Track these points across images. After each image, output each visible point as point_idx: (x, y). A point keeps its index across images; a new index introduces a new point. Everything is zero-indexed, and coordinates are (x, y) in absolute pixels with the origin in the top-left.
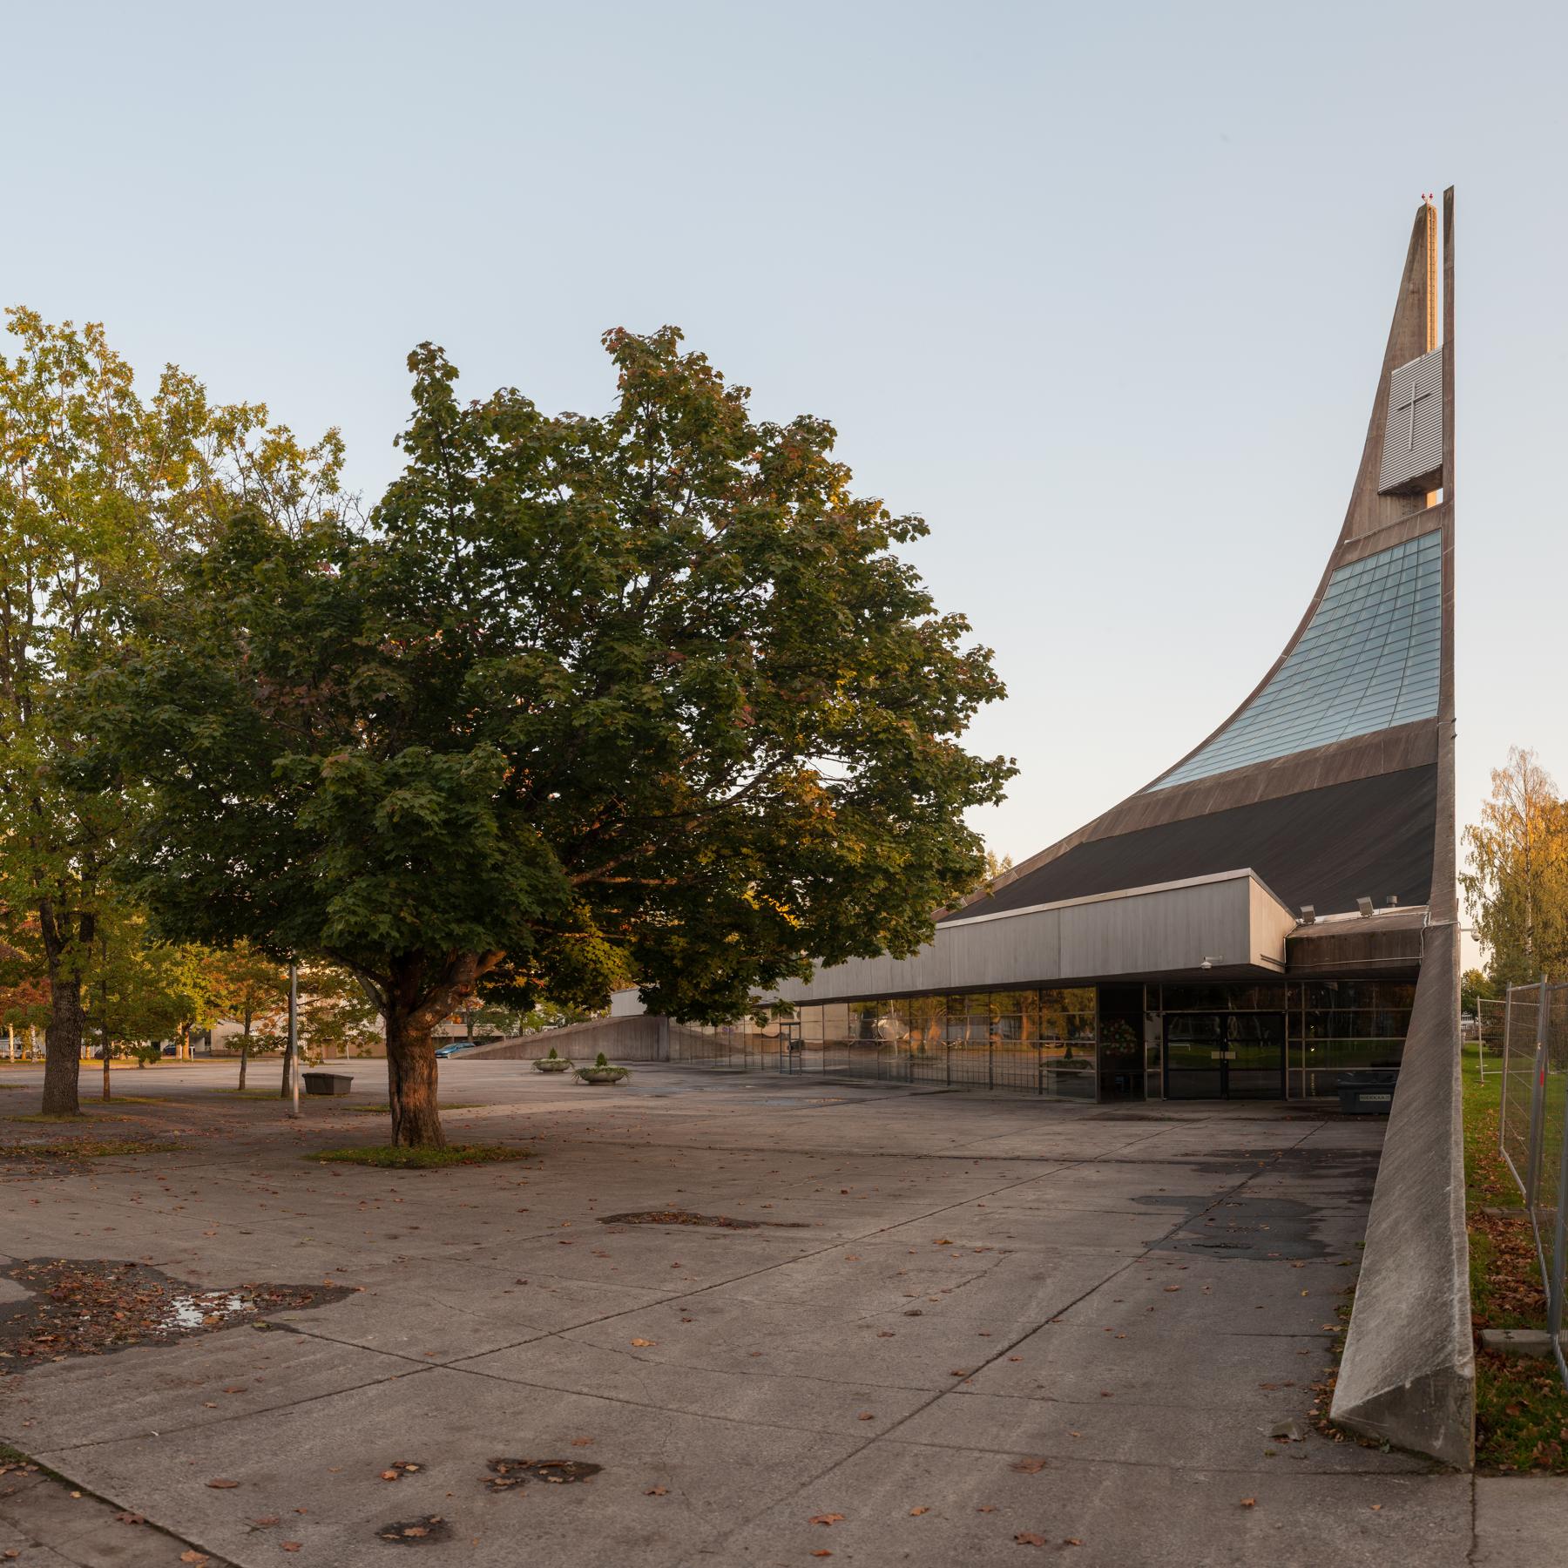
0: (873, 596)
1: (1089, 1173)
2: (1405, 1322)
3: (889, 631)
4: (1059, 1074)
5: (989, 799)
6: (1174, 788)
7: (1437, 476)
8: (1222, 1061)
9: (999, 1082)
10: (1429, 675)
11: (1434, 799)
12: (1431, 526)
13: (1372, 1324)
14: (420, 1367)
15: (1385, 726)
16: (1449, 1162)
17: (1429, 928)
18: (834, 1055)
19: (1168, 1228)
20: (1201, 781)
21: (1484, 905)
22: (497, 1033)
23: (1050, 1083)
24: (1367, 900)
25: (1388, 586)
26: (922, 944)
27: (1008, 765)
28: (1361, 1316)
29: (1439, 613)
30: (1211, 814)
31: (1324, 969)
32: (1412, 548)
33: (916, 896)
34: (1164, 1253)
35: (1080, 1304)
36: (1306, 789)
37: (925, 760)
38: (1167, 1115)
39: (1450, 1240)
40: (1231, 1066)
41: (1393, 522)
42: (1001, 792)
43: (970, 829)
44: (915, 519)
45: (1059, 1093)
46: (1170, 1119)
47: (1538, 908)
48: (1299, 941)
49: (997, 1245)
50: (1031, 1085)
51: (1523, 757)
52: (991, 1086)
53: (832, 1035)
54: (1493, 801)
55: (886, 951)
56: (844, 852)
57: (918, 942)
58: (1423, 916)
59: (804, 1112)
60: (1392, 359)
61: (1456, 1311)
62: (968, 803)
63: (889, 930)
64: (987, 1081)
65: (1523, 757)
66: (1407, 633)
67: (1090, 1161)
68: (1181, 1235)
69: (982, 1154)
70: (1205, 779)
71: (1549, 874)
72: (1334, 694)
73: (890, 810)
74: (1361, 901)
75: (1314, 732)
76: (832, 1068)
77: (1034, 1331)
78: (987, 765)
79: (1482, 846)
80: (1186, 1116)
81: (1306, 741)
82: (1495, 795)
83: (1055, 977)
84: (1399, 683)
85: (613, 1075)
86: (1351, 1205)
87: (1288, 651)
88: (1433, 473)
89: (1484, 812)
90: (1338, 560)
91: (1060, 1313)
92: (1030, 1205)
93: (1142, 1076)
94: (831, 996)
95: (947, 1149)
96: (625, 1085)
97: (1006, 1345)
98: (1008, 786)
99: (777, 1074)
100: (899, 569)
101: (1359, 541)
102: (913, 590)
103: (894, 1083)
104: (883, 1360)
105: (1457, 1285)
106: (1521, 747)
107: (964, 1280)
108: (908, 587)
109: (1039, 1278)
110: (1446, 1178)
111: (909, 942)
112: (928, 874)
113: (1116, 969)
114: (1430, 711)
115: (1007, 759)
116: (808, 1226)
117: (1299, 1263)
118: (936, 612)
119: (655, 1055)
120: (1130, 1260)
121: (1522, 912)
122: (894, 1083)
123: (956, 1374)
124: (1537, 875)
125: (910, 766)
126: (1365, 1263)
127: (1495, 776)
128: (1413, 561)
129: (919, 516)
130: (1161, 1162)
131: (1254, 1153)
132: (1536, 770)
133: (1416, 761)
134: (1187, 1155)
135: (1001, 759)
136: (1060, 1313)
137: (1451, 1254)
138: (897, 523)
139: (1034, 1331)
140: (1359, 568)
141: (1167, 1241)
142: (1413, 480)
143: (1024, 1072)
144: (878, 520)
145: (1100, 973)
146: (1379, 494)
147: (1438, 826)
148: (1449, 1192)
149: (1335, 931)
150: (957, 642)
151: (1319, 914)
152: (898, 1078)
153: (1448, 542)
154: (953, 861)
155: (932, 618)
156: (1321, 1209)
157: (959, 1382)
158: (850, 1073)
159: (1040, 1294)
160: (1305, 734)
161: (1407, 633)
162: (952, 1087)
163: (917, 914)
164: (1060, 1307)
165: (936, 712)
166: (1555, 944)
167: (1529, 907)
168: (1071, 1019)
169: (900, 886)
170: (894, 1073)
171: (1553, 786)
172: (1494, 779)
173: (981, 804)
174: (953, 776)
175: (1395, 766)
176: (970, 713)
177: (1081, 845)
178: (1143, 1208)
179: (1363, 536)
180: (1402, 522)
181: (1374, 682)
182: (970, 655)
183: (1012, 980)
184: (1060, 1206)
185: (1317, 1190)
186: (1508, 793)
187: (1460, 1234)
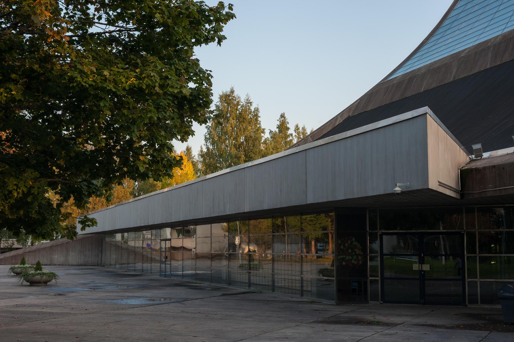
5: (213, 40)
6: (403, 75)
14: (377, 332)
20: (419, 69)
22: (16, 245)
30: (425, 92)
31: (489, 194)
36: (482, 69)
42: (222, 33)
46: (378, 323)
48: (471, 170)
52: (273, 288)
56: (76, 74)
62: (198, 43)
70: (421, 68)
75: (488, 29)
78: (211, 9)
81: (482, 36)
83: (304, 203)
85: (45, 278)
93: (366, 283)
96: (54, 286)
98: (227, 29)
115: (226, 4)
119: (100, 262)
149: (495, 162)
151: (485, 151)
154: (172, 87)
160: (481, 32)
162: (252, 289)
173: (207, 43)
177: (349, 117)
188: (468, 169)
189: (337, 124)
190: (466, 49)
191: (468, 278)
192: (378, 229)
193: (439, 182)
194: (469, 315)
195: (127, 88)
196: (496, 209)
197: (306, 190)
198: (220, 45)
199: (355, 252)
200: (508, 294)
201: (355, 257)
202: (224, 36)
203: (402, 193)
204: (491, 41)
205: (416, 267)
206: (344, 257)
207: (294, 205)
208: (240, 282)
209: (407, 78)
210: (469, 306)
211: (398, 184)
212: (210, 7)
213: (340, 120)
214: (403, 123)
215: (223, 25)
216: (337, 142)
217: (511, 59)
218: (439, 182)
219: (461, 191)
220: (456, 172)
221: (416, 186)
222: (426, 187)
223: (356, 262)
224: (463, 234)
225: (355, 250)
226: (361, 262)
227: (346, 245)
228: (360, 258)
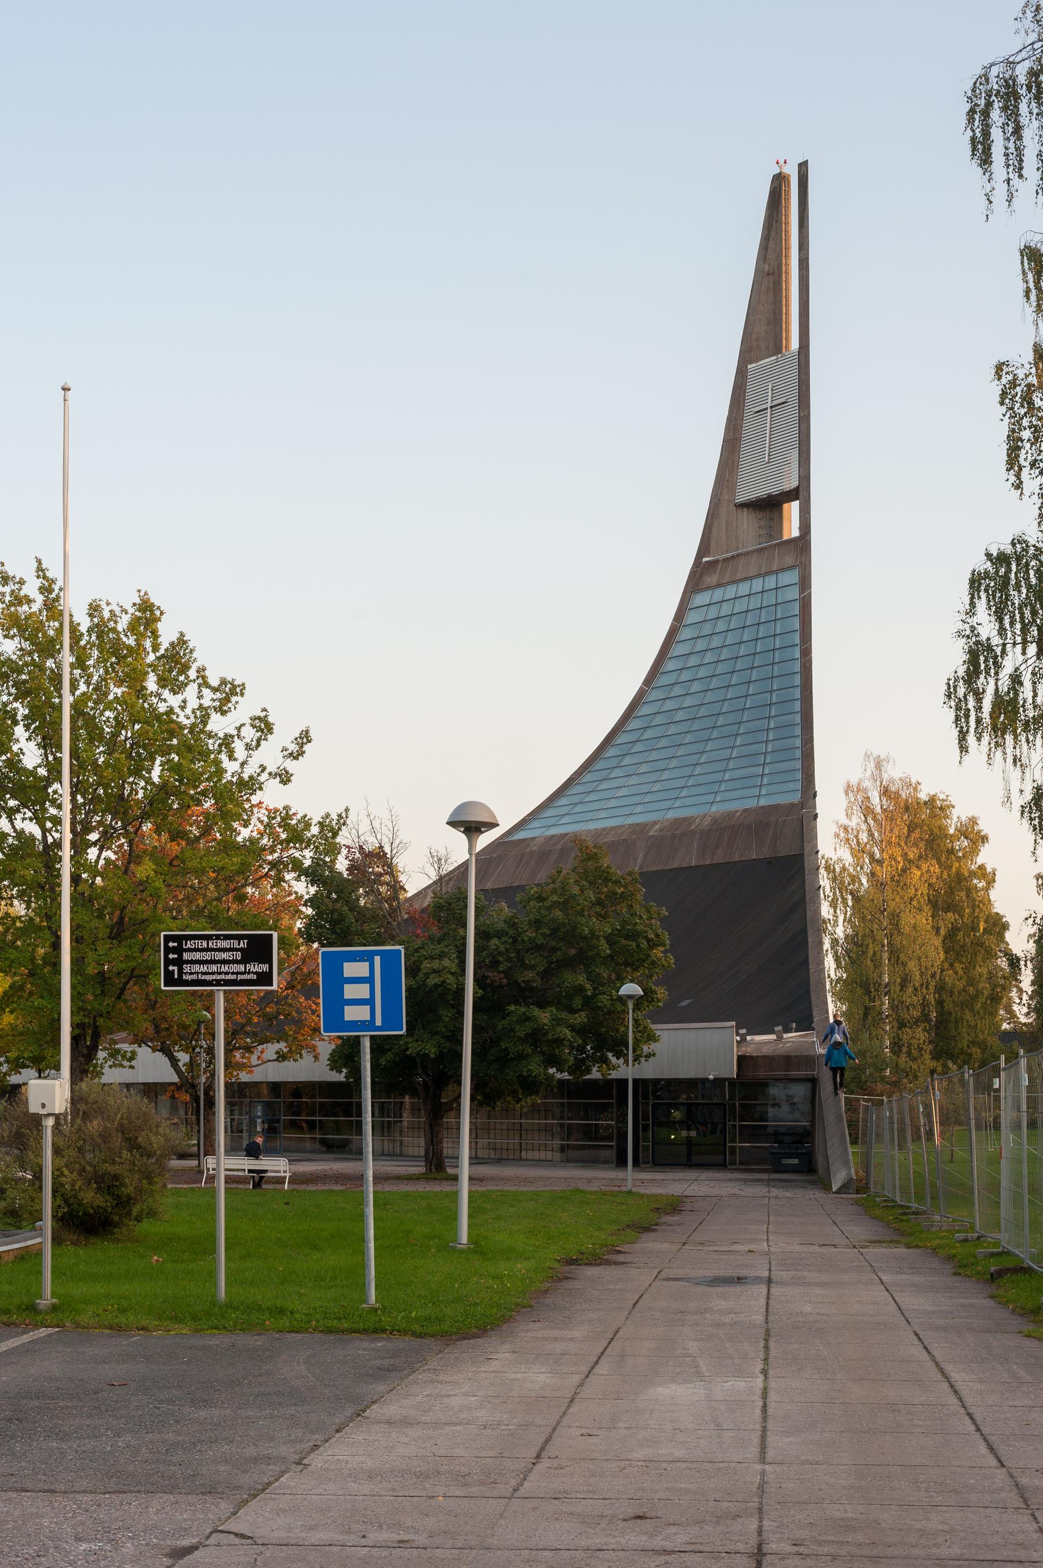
36: (685, 865)
51: (879, 765)
54: (845, 821)
60: (749, 352)
65: (879, 765)
87: (649, 681)
89: (837, 836)
90: (696, 581)
101: (716, 562)
114: (796, 797)
121: (877, 964)
153: (805, 583)
172: (847, 794)
175: (765, 853)
210: (729, 1167)
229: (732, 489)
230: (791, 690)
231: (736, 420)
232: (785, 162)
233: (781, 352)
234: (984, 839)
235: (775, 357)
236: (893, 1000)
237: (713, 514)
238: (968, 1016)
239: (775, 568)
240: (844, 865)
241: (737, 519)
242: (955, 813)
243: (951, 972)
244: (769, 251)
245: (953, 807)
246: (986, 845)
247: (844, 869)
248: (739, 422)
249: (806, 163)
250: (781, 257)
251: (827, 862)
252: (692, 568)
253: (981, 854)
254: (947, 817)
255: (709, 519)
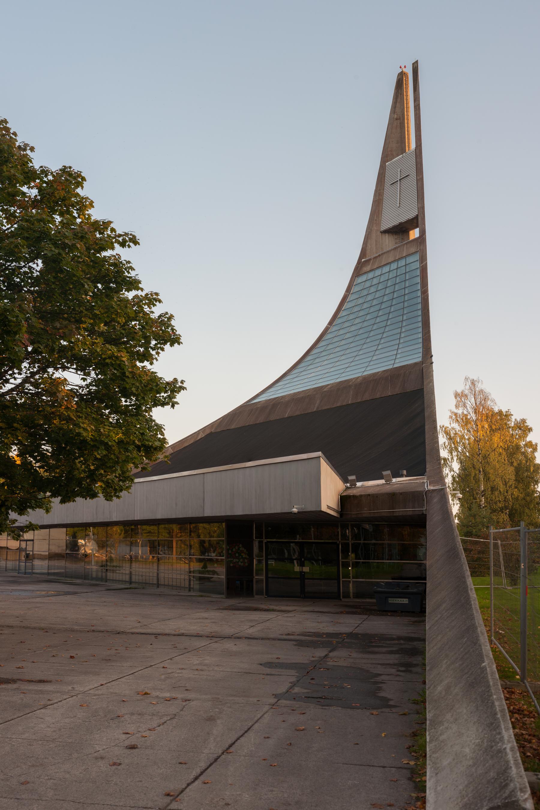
0: (104, 276)
1: (229, 645)
2: (471, 763)
3: (113, 298)
4: (201, 579)
5: (167, 404)
6: (267, 401)
7: (415, 221)
8: (301, 572)
9: (162, 583)
10: (415, 336)
11: (423, 411)
12: (413, 250)
13: (445, 763)
15: (391, 367)
16: (480, 646)
17: (429, 491)
18: (56, 563)
19: (287, 685)
21: (453, 476)
23: (196, 585)
24: (388, 472)
25: (389, 285)
26: (123, 492)
27: (180, 384)
28: (434, 755)
29: (419, 300)
30: (289, 418)
32: (402, 263)
33: (124, 461)
34: (288, 702)
35: (242, 739)
36: (344, 404)
37: (133, 377)
38: (272, 607)
39: (493, 703)
40: (306, 577)
41: (390, 249)
42: (175, 400)
43: (157, 422)
44: (131, 235)
45: (201, 590)
46: (274, 610)
47: (487, 479)
49: (180, 696)
50: (183, 585)
53: (55, 549)
55: (101, 495)
56: (81, 430)
57: (121, 490)
58: (424, 483)
59: (38, 600)
60: (387, 156)
61: (510, 756)
62: (155, 405)
63: (103, 481)
64: (155, 582)
65: (473, 383)
66: (401, 312)
67: (229, 637)
68: (296, 690)
69: (159, 631)
71: (492, 456)
72: (359, 348)
73: (106, 407)
74: (384, 473)
76: (53, 571)
77: (216, 760)
78: (168, 383)
79: (450, 439)
80: (283, 608)
81: (343, 375)
82: (457, 407)
83: (201, 515)
84: (397, 342)
86: (399, 673)
87: (331, 323)
88: (413, 219)
89: (451, 417)
90: (358, 271)
91: (230, 746)
92: (196, 667)
93: (252, 581)
94: (56, 523)
95: (136, 627)
97: (198, 771)
98: (179, 397)
99: (16, 574)
100: (121, 262)
102: (129, 275)
103: (94, 582)
104: (116, 784)
105: (506, 737)
106: (471, 378)
107: (162, 721)
108: (126, 274)
109: (211, 719)
110: (481, 657)
111: (115, 490)
112: (131, 448)
113: (239, 511)
114: (417, 358)
115: (179, 380)
116: (50, 682)
117: (375, 712)
118: (142, 290)
120: (266, 708)
121: (477, 481)
122: (94, 582)
123: (168, 795)
124: (485, 457)
125: (124, 380)
126: (429, 716)
127: (456, 395)
128: (403, 270)
129: (133, 233)
130: (274, 639)
131: (329, 635)
132: (481, 391)
133: (411, 387)
134: (289, 634)
135: (176, 380)
136: (230, 746)
137: (496, 714)
138: (120, 236)
139: (216, 760)
140: (371, 275)
141: (286, 695)
142: (401, 224)
143: (178, 577)
144: (109, 232)
145: (229, 514)
146: (381, 232)
147: (427, 427)
148: (485, 667)
149: (370, 491)
150: (153, 309)
152: (97, 579)
153: (423, 259)
154: (148, 440)
155: (139, 293)
156: (381, 675)
157: (171, 801)
158: (66, 575)
159: (215, 732)
161: (401, 312)
162: (133, 585)
163: (123, 472)
164: (230, 742)
165: (138, 349)
166: (500, 501)
167: (481, 477)
168: (202, 543)
169: (114, 455)
170: (94, 575)
171: (493, 401)
172: (456, 397)
174: (148, 388)
175: (398, 390)
176: (159, 351)
177: (211, 434)
178: (268, 671)
179: (372, 257)
180: (395, 249)
181: (382, 341)
182: (160, 316)
183: (174, 517)
184: (216, 668)
185: (374, 662)
186: (465, 406)
187: (499, 699)
188: (346, 496)
189: (199, 438)
190: (328, 385)
191: (342, 578)
192: (264, 538)
193: (327, 506)
194: (346, 606)
195: (117, 441)
196: (365, 525)
197: (204, 506)
198: (173, 408)
199: (242, 556)
200: (380, 589)
201: (241, 560)
202: (177, 402)
203: (298, 512)
204: (352, 381)
205: (297, 569)
206: (232, 559)
207: (190, 516)
208: (113, 580)
209: (271, 404)
210: (343, 600)
211: (295, 506)
212: (167, 381)
213: (202, 435)
214: (299, 462)
215: (176, 394)
216: (236, 470)
217: (371, 398)
218: (327, 506)
219: (341, 512)
220: (337, 497)
221: (310, 507)
222: (319, 510)
223: (242, 564)
224: (339, 544)
225: (242, 554)
226: (247, 564)
227: (234, 550)
228: (246, 561)
229: (379, 224)
230: (415, 312)
231: (380, 190)
232: (405, 67)
233: (405, 152)
234: (530, 430)
235: (401, 156)
236: (487, 498)
237: (368, 237)
238: (527, 510)
239: (404, 255)
240: (456, 431)
241: (382, 239)
242: (513, 418)
243: (516, 490)
244: (397, 108)
245: (512, 415)
246: (531, 432)
247: (456, 434)
248: (381, 191)
249: (417, 62)
250: (404, 111)
251: (445, 429)
252: (356, 265)
253: (528, 437)
254: (509, 420)
255: (366, 240)
